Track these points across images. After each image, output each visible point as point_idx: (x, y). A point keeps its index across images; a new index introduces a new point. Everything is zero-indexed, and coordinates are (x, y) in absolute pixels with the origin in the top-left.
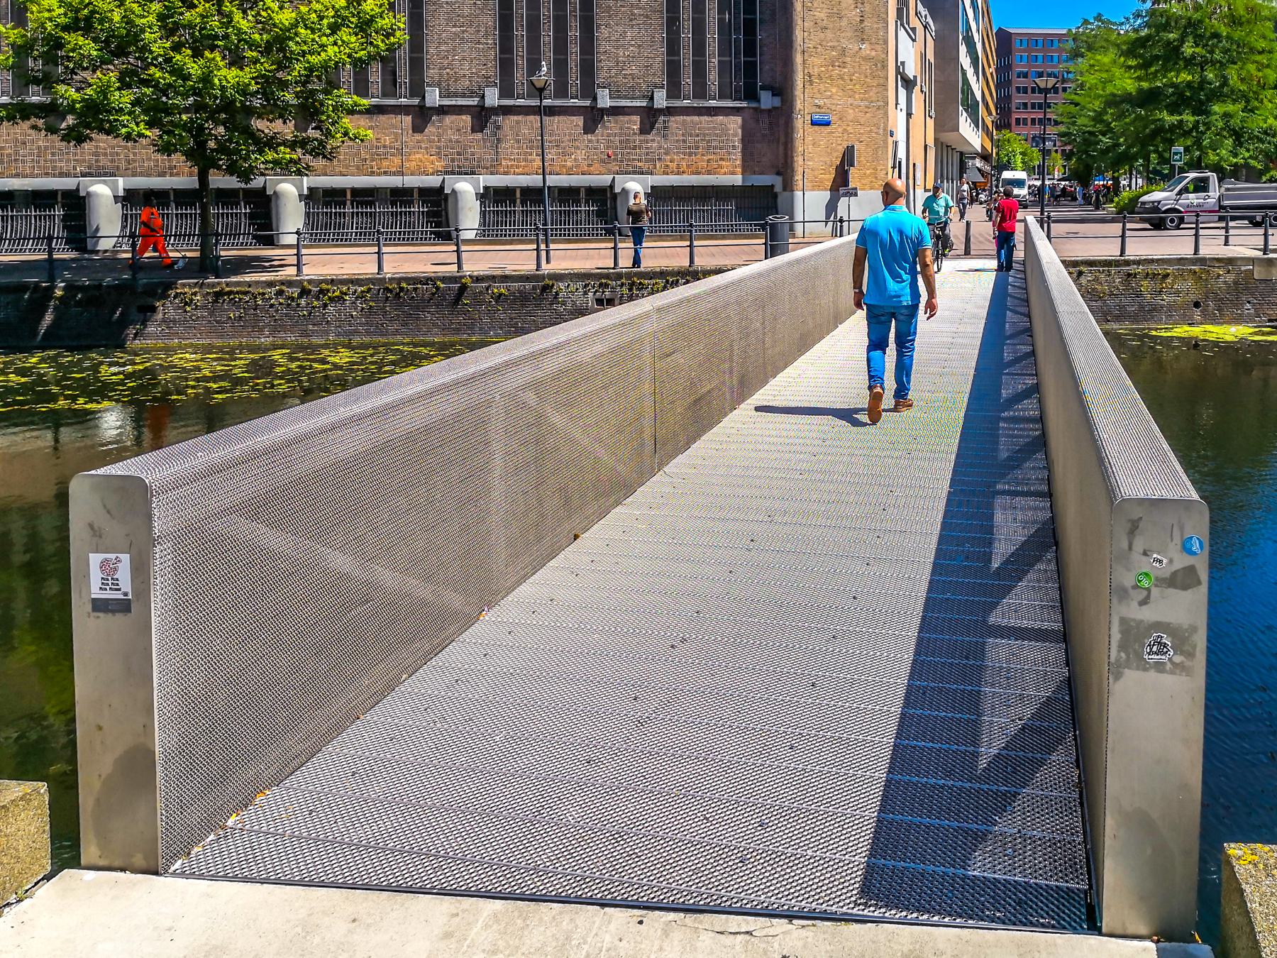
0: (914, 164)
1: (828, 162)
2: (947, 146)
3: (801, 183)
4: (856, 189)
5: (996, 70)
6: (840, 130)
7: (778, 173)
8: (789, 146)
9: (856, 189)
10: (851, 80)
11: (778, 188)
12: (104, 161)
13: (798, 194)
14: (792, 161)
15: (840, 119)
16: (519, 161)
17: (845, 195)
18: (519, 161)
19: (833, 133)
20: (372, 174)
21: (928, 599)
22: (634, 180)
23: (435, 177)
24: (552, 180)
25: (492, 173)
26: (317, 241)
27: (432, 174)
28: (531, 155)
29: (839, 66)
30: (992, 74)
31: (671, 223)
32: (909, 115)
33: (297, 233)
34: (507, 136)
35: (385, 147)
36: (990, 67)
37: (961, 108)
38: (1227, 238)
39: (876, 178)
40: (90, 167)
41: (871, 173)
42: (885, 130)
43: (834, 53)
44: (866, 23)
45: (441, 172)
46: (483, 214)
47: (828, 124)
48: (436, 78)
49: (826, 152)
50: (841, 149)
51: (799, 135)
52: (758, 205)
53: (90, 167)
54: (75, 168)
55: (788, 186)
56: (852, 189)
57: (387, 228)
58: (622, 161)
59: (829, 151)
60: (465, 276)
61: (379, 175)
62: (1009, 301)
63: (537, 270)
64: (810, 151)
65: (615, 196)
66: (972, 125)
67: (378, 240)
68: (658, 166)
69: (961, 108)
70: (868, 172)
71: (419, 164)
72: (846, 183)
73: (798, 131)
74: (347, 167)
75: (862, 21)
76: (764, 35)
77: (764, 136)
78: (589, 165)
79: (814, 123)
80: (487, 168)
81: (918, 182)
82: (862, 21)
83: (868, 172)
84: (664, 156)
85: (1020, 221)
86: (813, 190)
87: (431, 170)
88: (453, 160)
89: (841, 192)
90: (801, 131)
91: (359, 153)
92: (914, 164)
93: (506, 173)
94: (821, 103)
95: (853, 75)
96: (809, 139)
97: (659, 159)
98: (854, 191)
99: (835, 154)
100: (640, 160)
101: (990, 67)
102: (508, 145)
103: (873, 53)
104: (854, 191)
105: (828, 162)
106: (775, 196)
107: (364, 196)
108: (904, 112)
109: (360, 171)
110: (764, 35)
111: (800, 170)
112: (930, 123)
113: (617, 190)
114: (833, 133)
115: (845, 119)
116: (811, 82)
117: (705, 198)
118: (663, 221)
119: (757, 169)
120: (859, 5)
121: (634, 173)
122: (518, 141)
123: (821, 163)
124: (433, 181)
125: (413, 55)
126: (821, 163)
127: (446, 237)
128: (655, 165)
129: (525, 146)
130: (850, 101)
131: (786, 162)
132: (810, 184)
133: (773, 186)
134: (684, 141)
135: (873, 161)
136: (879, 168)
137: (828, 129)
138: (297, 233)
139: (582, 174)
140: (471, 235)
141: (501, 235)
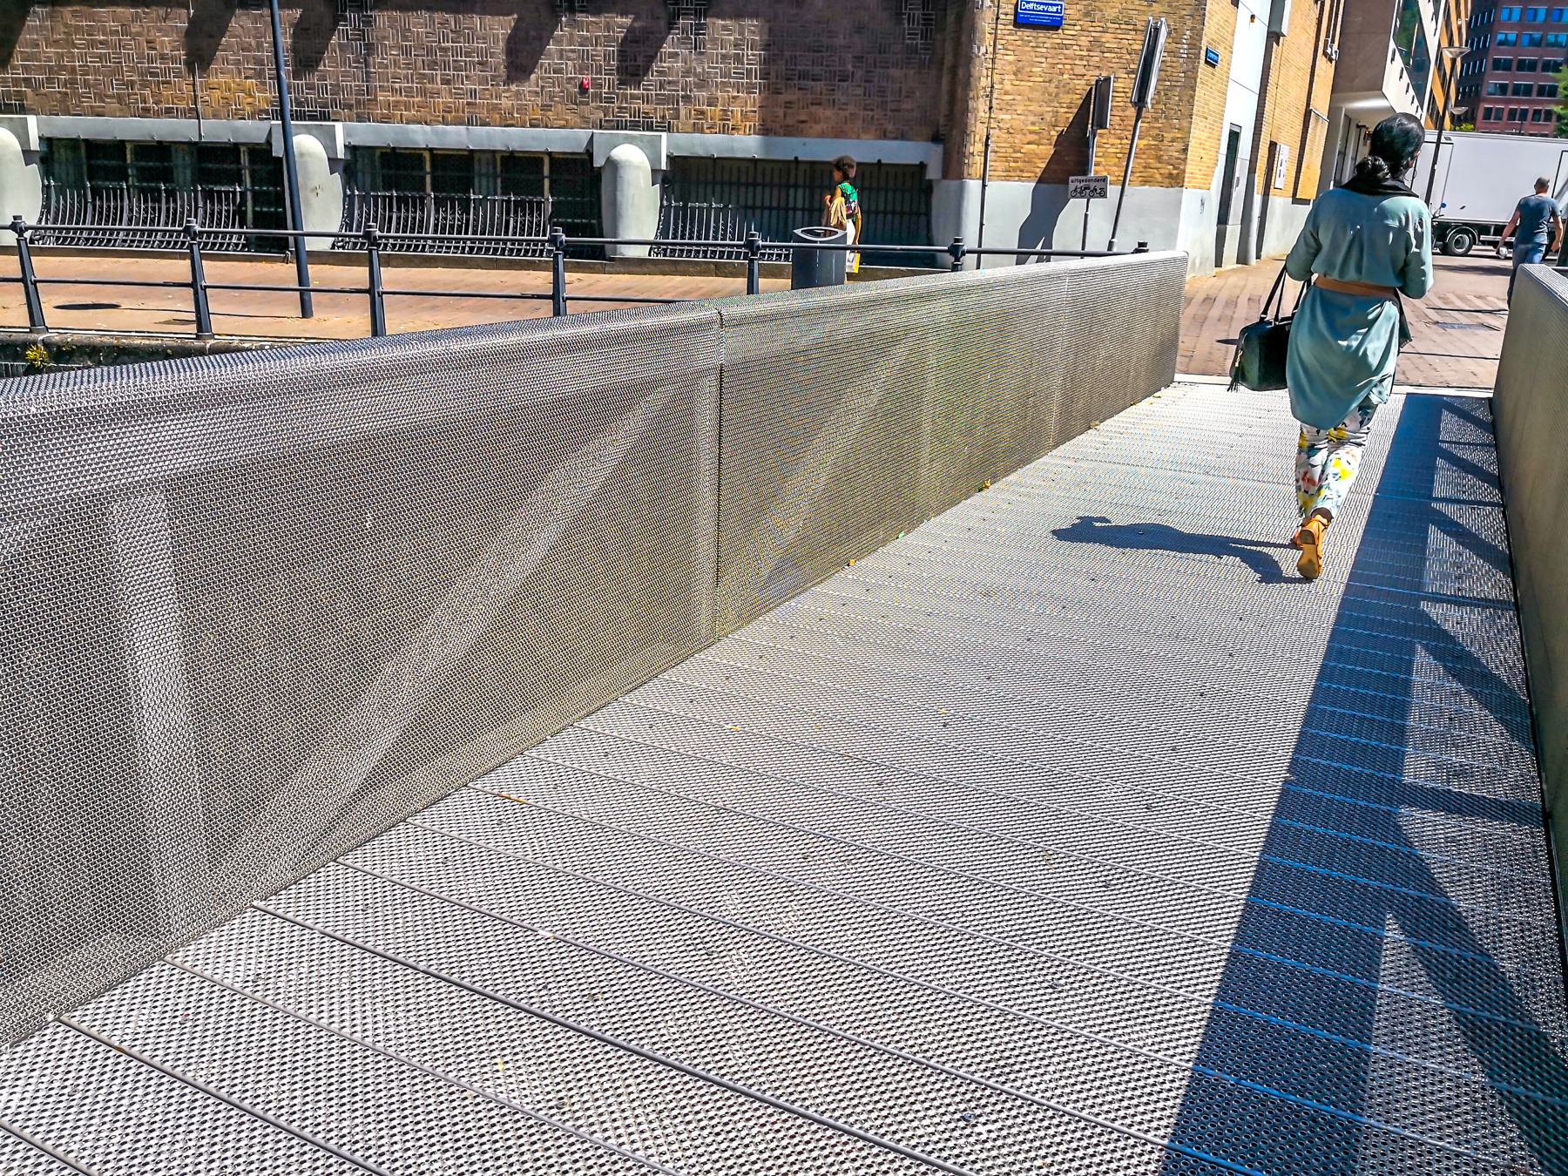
0: (1273, 145)
1: (1048, 117)
2: (1358, 126)
3: (979, 160)
4: (1104, 179)
5: (1469, 24)
6: (1084, 41)
7: (936, 138)
8: (961, 72)
9: (1104, 179)
11: (933, 173)
13: (973, 186)
14: (966, 110)
15: (1087, 14)
16: (409, 92)
17: (1080, 193)
18: (409, 92)
19: (1067, 47)
20: (146, 112)
21: (1261, 867)
22: (630, 140)
23: (257, 123)
25: (360, 119)
26: (67, 245)
27: (252, 116)
28: (432, 80)
30: (1460, 28)
31: (506, 233)
32: (1274, 36)
34: (384, 38)
35: (163, 57)
36: (1459, 16)
37: (1392, 45)
39: (1159, 158)
41: (1149, 147)
42: (1194, 45)
45: (267, 112)
46: (348, 200)
47: (1054, 25)
49: (1045, 91)
50: (1082, 86)
51: (984, 47)
52: (767, 203)
55: (954, 166)
56: (1097, 180)
57: (92, 223)
58: (609, 100)
59: (1052, 89)
60: (35, 343)
61: (158, 114)
62: (1444, 482)
63: (198, 337)
64: (1008, 87)
65: (596, 175)
66: (1411, 92)
67: (191, 247)
68: (683, 112)
69: (1392, 45)
71: (227, 94)
72: (1083, 166)
73: (982, 40)
74: (101, 97)
77: (913, 50)
78: (546, 108)
79: (1020, 22)
80: (350, 107)
81: (1278, 182)
84: (696, 93)
85: (1305, 202)
86: (1007, 178)
87: (248, 108)
89: (1072, 186)
90: (989, 39)
91: (117, 71)
92: (1273, 145)
93: (386, 119)
96: (1006, 60)
97: (687, 99)
98: (1099, 185)
99: (1066, 99)
101: (1459, 16)
102: (387, 57)
104: (1099, 185)
105: (1048, 117)
106: (928, 189)
107: (157, 155)
108: (1260, 30)
109: (127, 107)
111: (979, 131)
112: (1326, 70)
113: (599, 162)
114: (1067, 47)
115: (1098, 15)
117: (714, 183)
118: (691, 232)
119: (890, 127)
121: (635, 126)
122: (406, 51)
123: (1032, 118)
124: (253, 130)
126: (1032, 118)
127: (275, 247)
128: (677, 110)
129: (420, 64)
131: (950, 116)
132: (1000, 166)
133: (922, 166)
135: (1156, 119)
136: (1168, 136)
137: (1055, 38)
139: (532, 126)
140: (324, 245)
141: (534, 251)
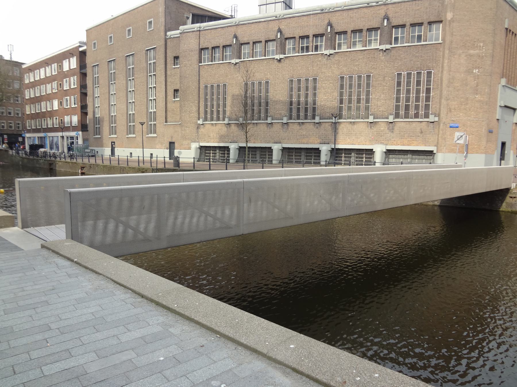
10: (470, 110)
12: (235, 139)
15: (463, 125)
24: (250, 145)
29: (464, 105)
33: (194, 158)
38: (244, 166)
40: (232, 140)
43: (462, 100)
44: (479, 87)
48: (319, 113)
53: (232, 140)
54: (229, 141)
70: (476, 146)
75: (477, 86)
76: (433, 94)
82: (477, 86)
83: (476, 146)
88: (323, 140)
94: (455, 119)
95: (471, 108)
100: (383, 140)
103: (482, 99)
110: (433, 94)
116: (450, 111)
120: (476, 80)
125: (397, 104)
130: (469, 118)
134: (399, 134)
138: (194, 158)
